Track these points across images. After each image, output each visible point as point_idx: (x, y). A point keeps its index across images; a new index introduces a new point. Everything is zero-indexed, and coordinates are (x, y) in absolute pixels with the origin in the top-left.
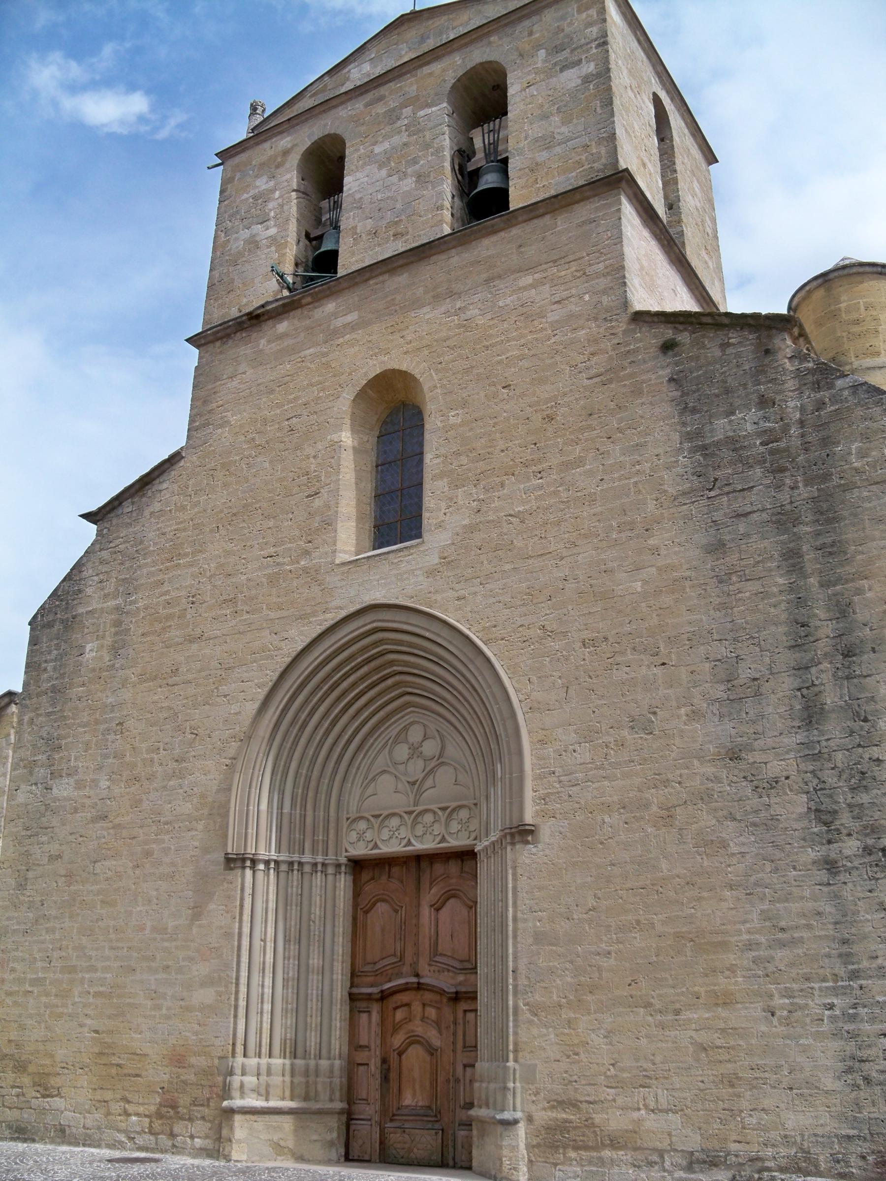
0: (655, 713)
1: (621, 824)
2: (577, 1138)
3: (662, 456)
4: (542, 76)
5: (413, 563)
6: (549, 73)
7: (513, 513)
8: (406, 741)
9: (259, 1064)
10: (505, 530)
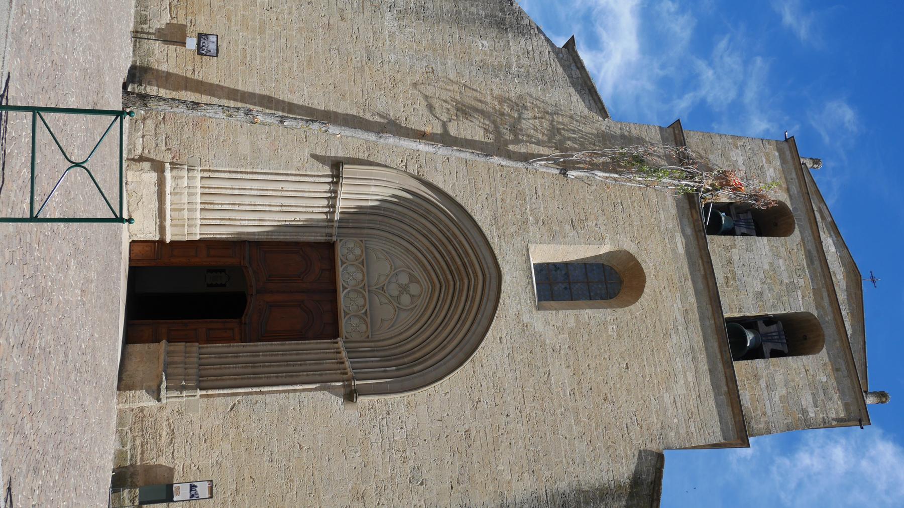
0: (422, 484)
1: (354, 465)
2: (149, 445)
3: (576, 479)
4: (811, 380)
5: (525, 303)
6: (812, 384)
7: (551, 375)
8: (411, 282)
9: (196, 187)
10: (541, 370)
